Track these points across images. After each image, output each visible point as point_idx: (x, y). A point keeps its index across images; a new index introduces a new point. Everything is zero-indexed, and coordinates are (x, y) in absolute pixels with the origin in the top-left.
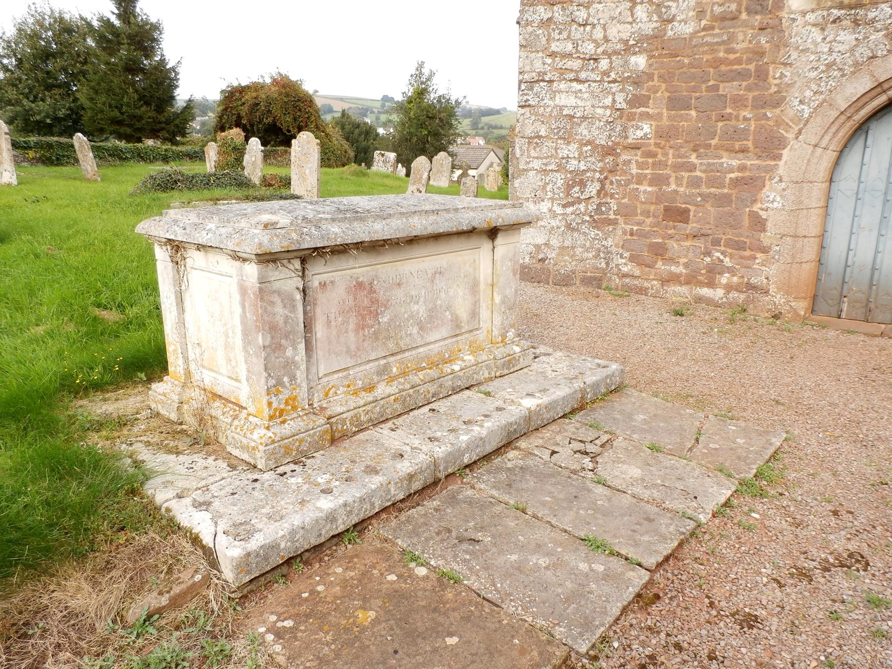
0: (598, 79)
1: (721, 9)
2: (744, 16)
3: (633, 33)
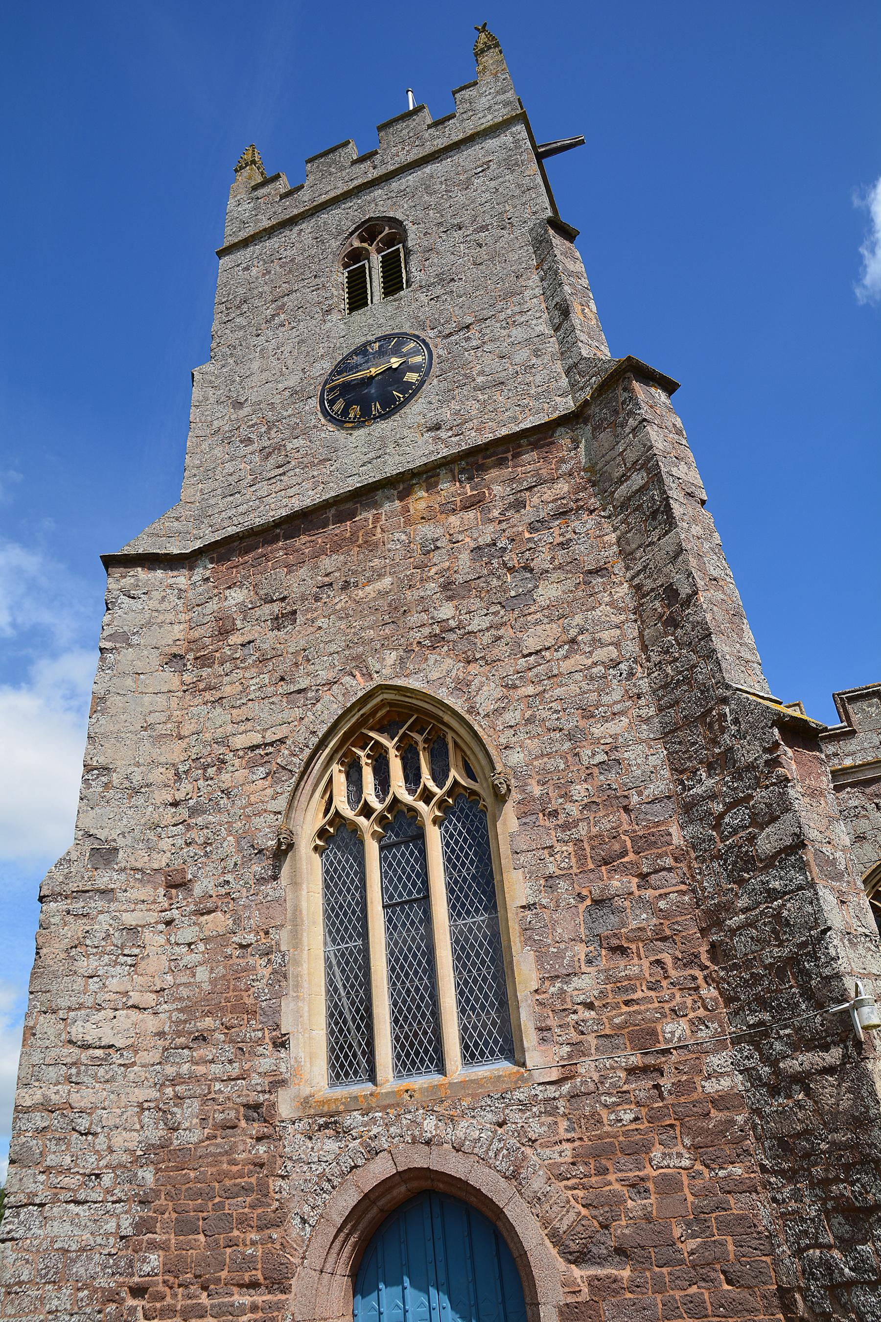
0: (100, 1199)
1: (222, 1116)
2: (243, 1124)
3: (140, 1142)
